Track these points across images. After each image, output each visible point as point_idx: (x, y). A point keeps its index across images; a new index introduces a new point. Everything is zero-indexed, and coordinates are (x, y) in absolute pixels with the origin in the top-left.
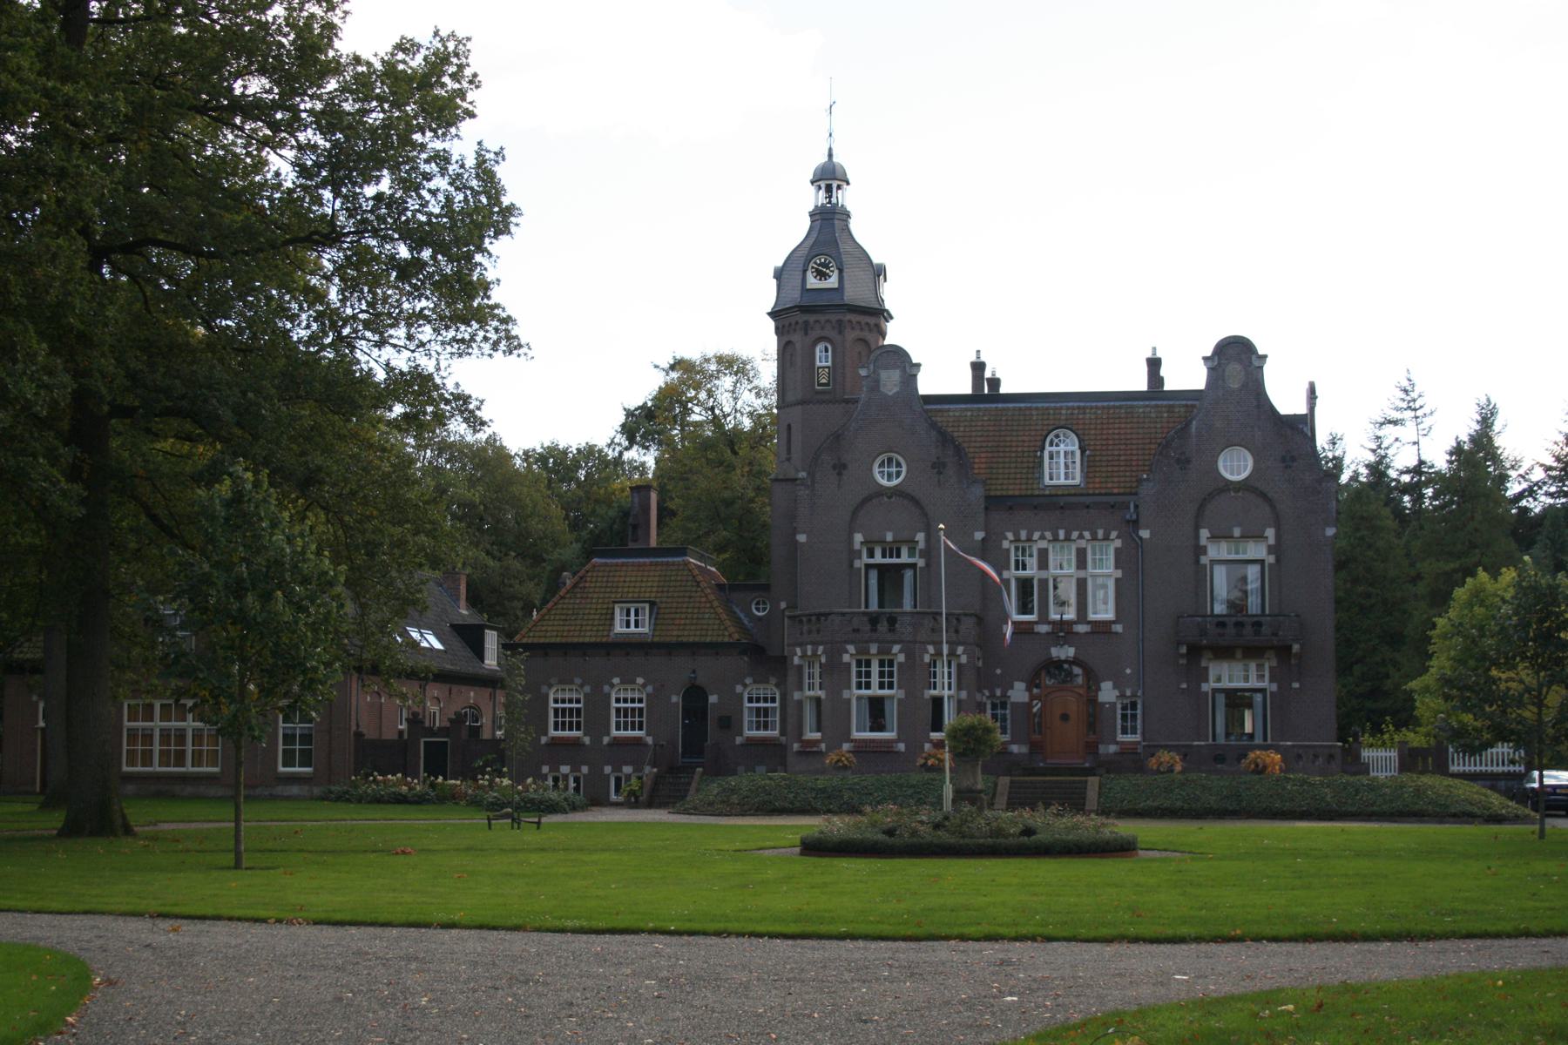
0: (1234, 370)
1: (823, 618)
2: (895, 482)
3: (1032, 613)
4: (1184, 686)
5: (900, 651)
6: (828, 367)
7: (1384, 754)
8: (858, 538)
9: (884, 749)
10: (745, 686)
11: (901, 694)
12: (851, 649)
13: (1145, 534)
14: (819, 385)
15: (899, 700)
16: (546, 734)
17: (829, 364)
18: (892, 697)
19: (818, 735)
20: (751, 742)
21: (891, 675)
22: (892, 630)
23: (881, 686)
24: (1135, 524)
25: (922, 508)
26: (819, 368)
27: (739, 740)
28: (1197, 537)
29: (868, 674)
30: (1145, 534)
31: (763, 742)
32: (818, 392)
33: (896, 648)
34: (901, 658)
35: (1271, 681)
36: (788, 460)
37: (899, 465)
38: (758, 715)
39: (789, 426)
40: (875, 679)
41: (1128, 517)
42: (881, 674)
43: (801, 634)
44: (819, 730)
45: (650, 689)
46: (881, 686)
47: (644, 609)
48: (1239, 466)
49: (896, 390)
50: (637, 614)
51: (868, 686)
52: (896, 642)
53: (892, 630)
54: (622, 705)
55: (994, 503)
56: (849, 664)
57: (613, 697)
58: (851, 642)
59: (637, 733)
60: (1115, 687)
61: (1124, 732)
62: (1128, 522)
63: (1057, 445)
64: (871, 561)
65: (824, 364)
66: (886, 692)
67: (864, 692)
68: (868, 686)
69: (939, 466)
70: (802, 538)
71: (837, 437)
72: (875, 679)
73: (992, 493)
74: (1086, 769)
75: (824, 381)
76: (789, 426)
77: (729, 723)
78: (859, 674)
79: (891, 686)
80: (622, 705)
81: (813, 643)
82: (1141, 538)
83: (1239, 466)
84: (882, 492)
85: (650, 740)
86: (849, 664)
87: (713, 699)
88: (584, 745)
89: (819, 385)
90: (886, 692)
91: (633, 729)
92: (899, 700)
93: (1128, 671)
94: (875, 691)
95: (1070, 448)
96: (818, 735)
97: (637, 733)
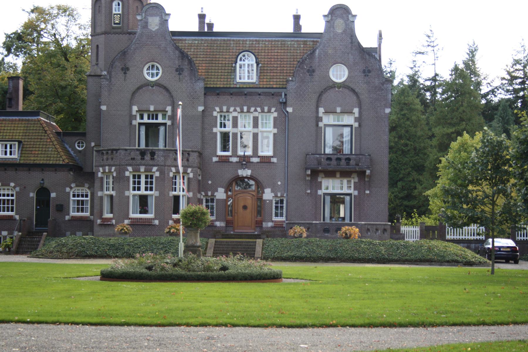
0: (339, 25)
1: (114, 152)
2: (155, 79)
3: (228, 151)
4: (309, 191)
5: (157, 171)
6: (120, 14)
7: (412, 229)
8: (135, 108)
9: (146, 224)
10: (71, 188)
11: (127, 193)
12: (130, 169)
13: (290, 110)
14: (115, 24)
15: (156, 197)
16: (68, 214)
17: (120, 12)
18: (152, 195)
19: (111, 216)
20: (74, 219)
21: (151, 183)
22: (152, 159)
23: (146, 189)
24: (285, 104)
25: (170, 93)
26: (114, 14)
27: (67, 218)
28: (131, 110)
29: (139, 183)
30: (290, 110)
31: (81, 219)
32: (113, 28)
33: (155, 169)
34: (157, 174)
35: (156, 190)
36: (97, 64)
37: (158, 69)
38: (78, 204)
39: (98, 46)
40: (143, 186)
41: (281, 100)
42: (146, 183)
43: (103, 160)
44: (111, 212)
45: (18, 189)
46: (146, 189)
47: (15, 145)
48: (340, 74)
49: (157, 28)
50: (11, 148)
51: (139, 189)
52: (154, 166)
53: (152, 159)
54: (76, 198)
55: (209, 91)
56: (129, 177)
57: (71, 194)
58: (130, 165)
59: (10, 213)
60: (272, 191)
61: (277, 215)
62: (281, 103)
63: (244, 60)
64: (142, 121)
65: (117, 12)
66: (148, 193)
67: (136, 192)
68: (139, 189)
69: (179, 71)
70: (104, 108)
71: (124, 53)
72: (143, 186)
73: (208, 86)
74: (256, 235)
75: (117, 22)
76: (98, 46)
77: (62, 208)
78: (134, 183)
79: (151, 189)
80: (76, 198)
81: (109, 165)
82: (287, 112)
83: (340, 74)
84: (148, 84)
85: (17, 217)
86: (129, 177)
87: (53, 195)
88: (15, 220)
89: (115, 24)
90: (148, 193)
91: (8, 211)
92: (156, 197)
93: (279, 183)
94: (143, 192)
95: (251, 63)
96: (111, 216)
97: (10, 213)
